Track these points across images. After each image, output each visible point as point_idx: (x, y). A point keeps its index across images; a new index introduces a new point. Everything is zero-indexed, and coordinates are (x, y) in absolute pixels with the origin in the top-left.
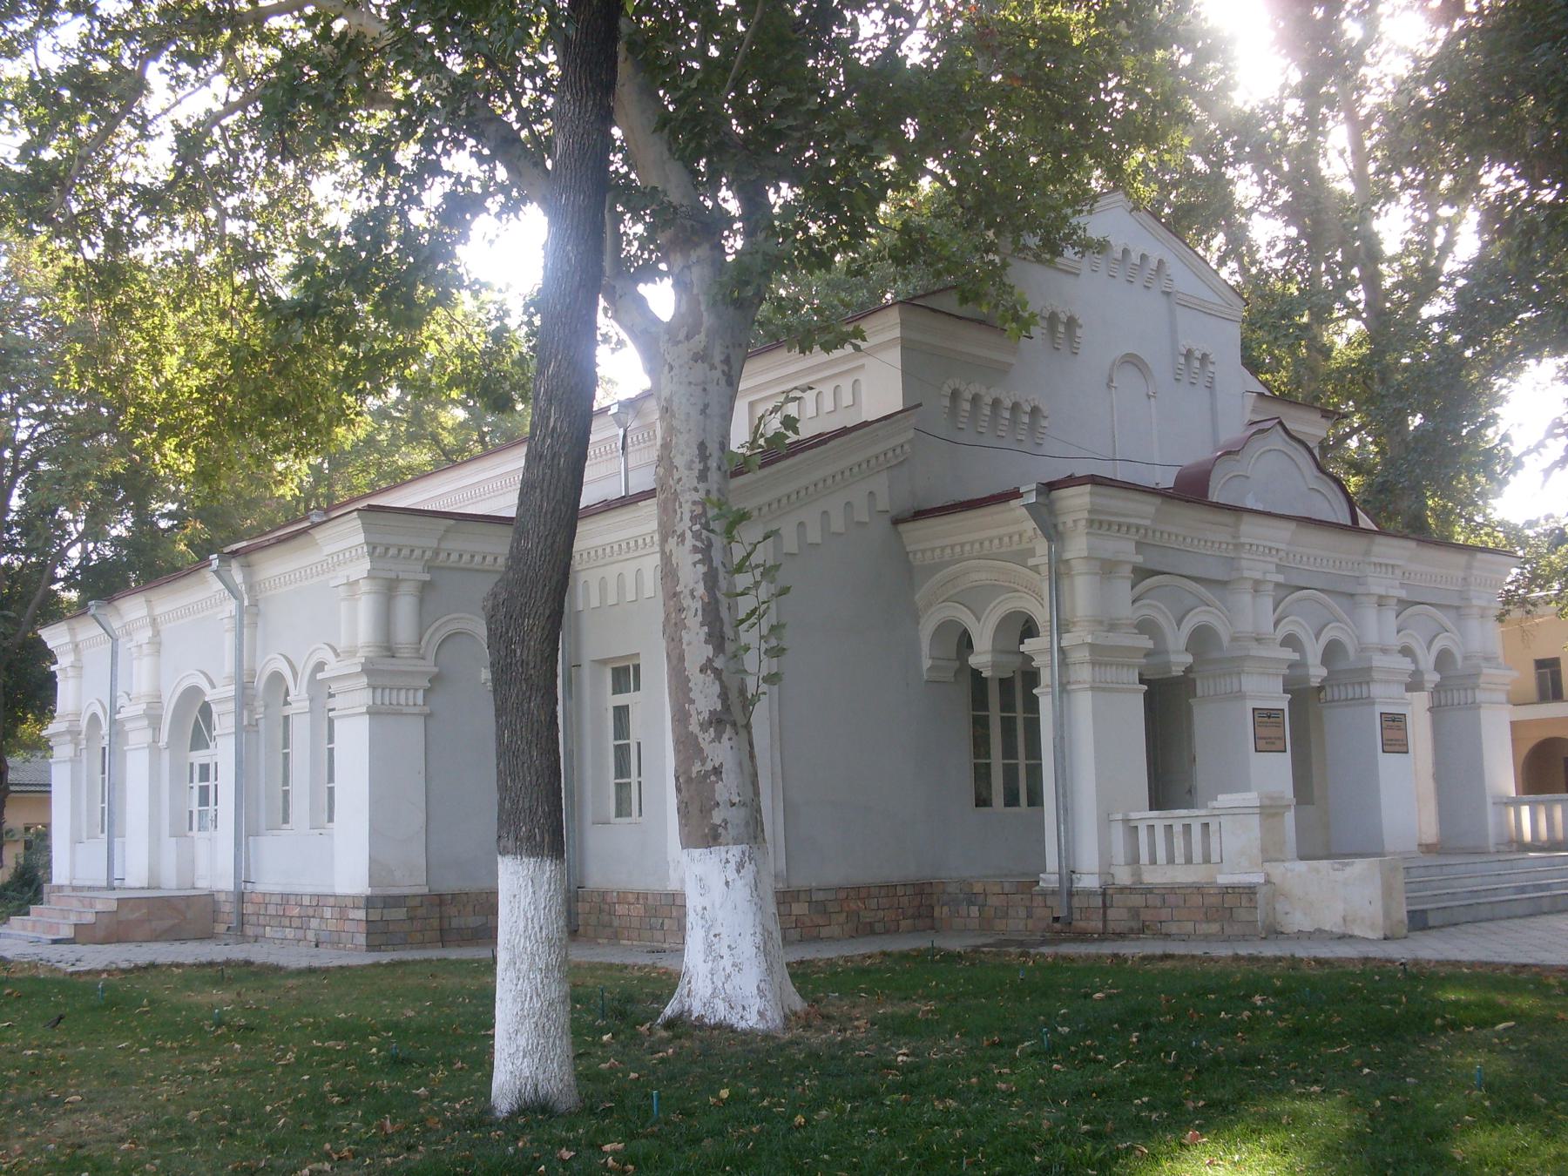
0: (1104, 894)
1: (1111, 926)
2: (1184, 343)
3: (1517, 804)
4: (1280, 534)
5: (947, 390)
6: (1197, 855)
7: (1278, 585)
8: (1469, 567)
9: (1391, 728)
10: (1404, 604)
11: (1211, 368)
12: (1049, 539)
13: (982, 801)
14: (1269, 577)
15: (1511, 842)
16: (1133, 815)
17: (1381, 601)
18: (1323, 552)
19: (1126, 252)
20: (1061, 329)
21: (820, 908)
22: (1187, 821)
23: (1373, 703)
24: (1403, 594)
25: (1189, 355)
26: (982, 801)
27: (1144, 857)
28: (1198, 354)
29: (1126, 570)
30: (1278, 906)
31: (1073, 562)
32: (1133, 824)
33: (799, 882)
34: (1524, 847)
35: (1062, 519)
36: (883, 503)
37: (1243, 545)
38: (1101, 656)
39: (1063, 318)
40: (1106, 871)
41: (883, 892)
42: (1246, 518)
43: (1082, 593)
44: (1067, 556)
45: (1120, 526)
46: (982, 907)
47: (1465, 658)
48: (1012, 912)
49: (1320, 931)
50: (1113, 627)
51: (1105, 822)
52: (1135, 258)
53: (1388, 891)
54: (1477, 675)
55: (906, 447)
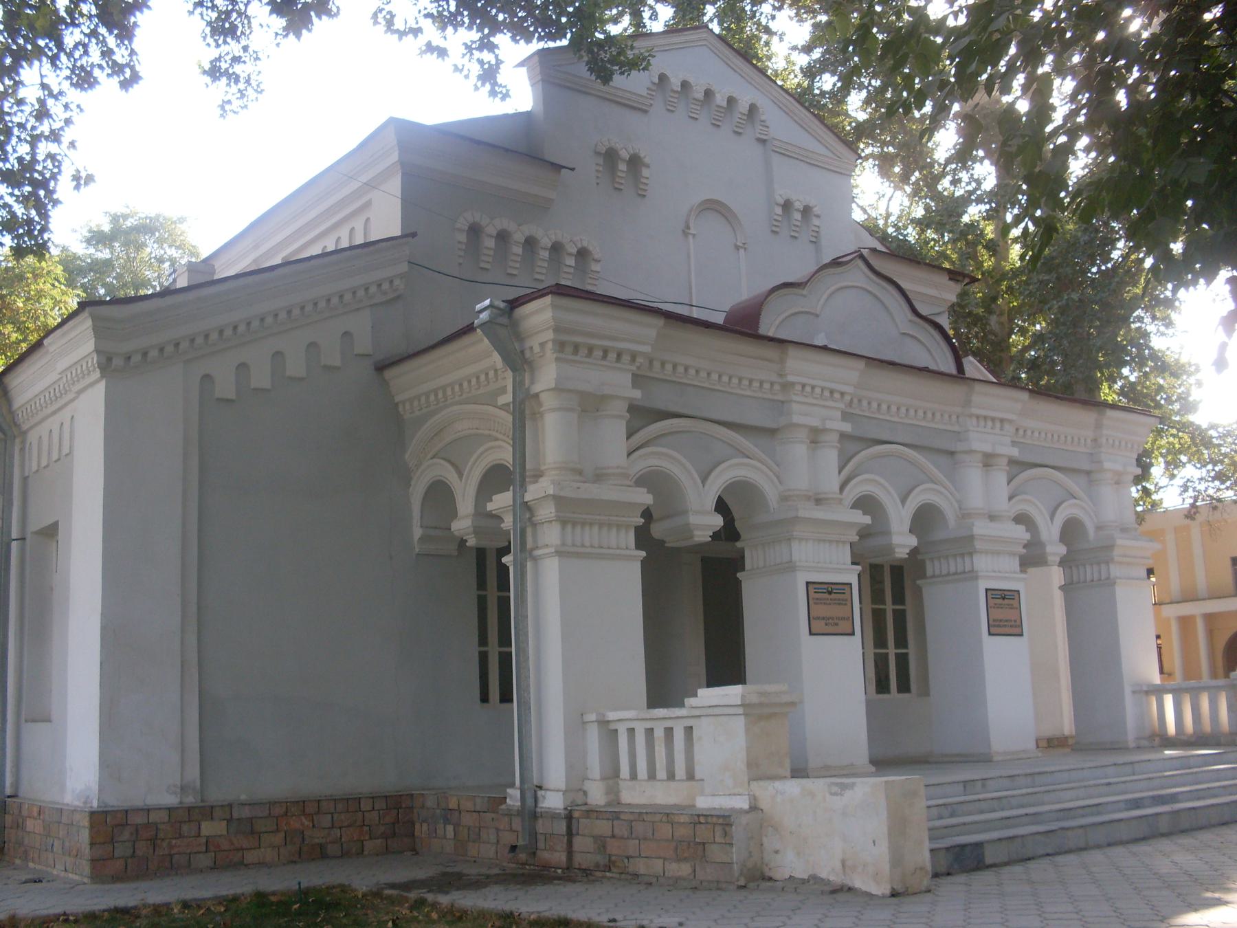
0: (569, 817)
1: (578, 859)
2: (781, 194)
3: (1159, 691)
4: (846, 375)
5: (463, 224)
6: (680, 771)
7: (843, 436)
8: (1098, 426)
9: (1000, 607)
10: (1017, 465)
11: (816, 222)
12: (514, 370)
13: (485, 698)
14: (829, 425)
15: (1152, 736)
16: (611, 716)
17: (988, 461)
18: (899, 400)
19: (708, 94)
20: (622, 167)
21: (250, 828)
22: (669, 724)
23: (977, 578)
24: (1015, 452)
25: (787, 206)
26: (485, 698)
27: (625, 771)
28: (798, 205)
29: (621, 408)
30: (765, 840)
31: (543, 397)
32: (612, 726)
33: (216, 795)
34: (1169, 742)
35: (528, 344)
36: (364, 344)
37: (793, 384)
38: (572, 512)
39: (625, 155)
40: (575, 787)
41: (340, 806)
42: (792, 352)
43: (553, 437)
44: (537, 388)
45: (606, 352)
46: (457, 826)
47: (1099, 528)
48: (484, 836)
49: (814, 879)
50: (599, 477)
51: (576, 726)
52: (720, 100)
53: (898, 826)
54: (1110, 547)
55: (397, 282)
